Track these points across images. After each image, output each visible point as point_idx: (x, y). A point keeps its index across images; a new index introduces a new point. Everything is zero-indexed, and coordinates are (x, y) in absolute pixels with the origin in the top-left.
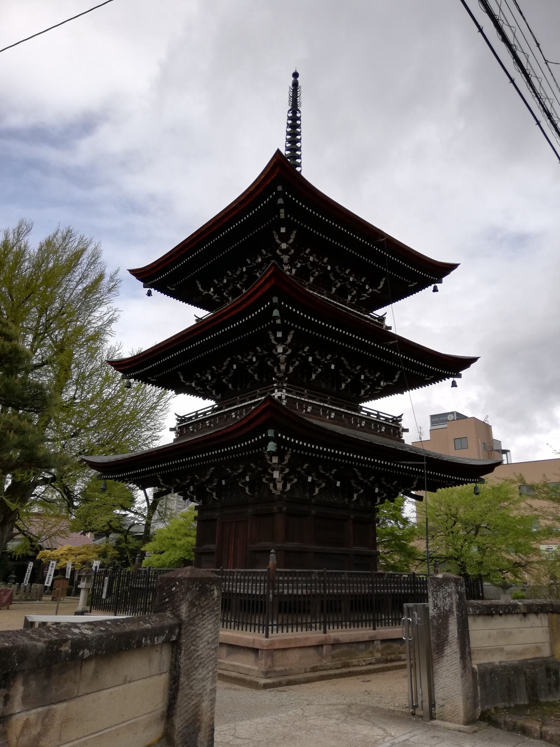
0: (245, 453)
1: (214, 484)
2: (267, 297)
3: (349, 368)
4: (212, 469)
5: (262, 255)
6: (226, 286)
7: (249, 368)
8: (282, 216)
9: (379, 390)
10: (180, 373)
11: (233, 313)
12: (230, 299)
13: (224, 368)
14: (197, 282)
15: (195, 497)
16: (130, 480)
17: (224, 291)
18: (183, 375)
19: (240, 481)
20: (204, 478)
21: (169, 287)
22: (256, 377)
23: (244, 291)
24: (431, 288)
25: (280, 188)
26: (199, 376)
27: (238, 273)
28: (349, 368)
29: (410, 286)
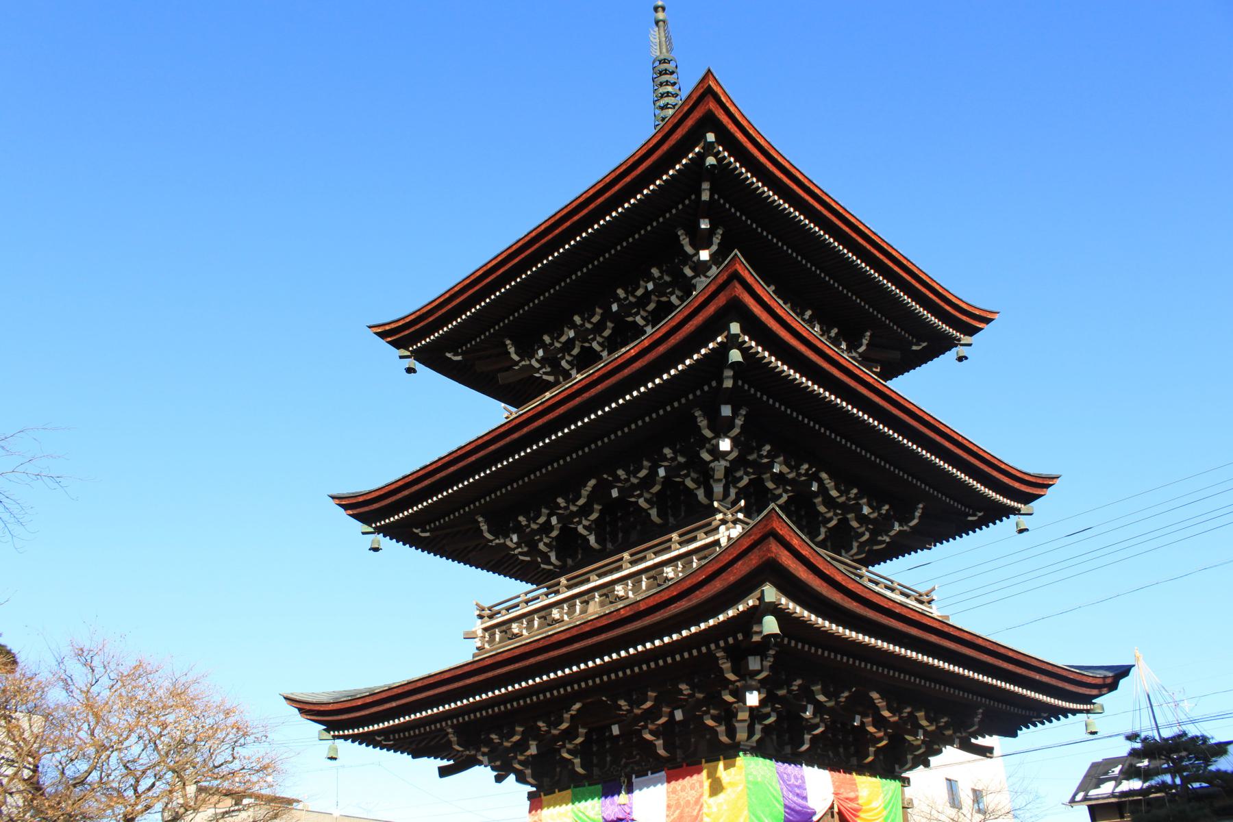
0: (609, 677)
1: (579, 740)
2: (717, 324)
3: (886, 714)
4: (578, 706)
5: (617, 299)
6: (569, 344)
7: (580, 523)
8: (705, 196)
9: (884, 542)
10: (480, 519)
11: (593, 392)
12: (605, 354)
13: (581, 502)
14: (508, 342)
15: (528, 772)
16: (387, 739)
17: (563, 358)
18: (487, 522)
19: (563, 746)
20: (638, 708)
21: (449, 355)
22: (592, 539)
23: (649, 330)
24: (951, 355)
25: (711, 137)
26: (524, 523)
27: (639, 292)
28: (886, 714)
29: (914, 348)
